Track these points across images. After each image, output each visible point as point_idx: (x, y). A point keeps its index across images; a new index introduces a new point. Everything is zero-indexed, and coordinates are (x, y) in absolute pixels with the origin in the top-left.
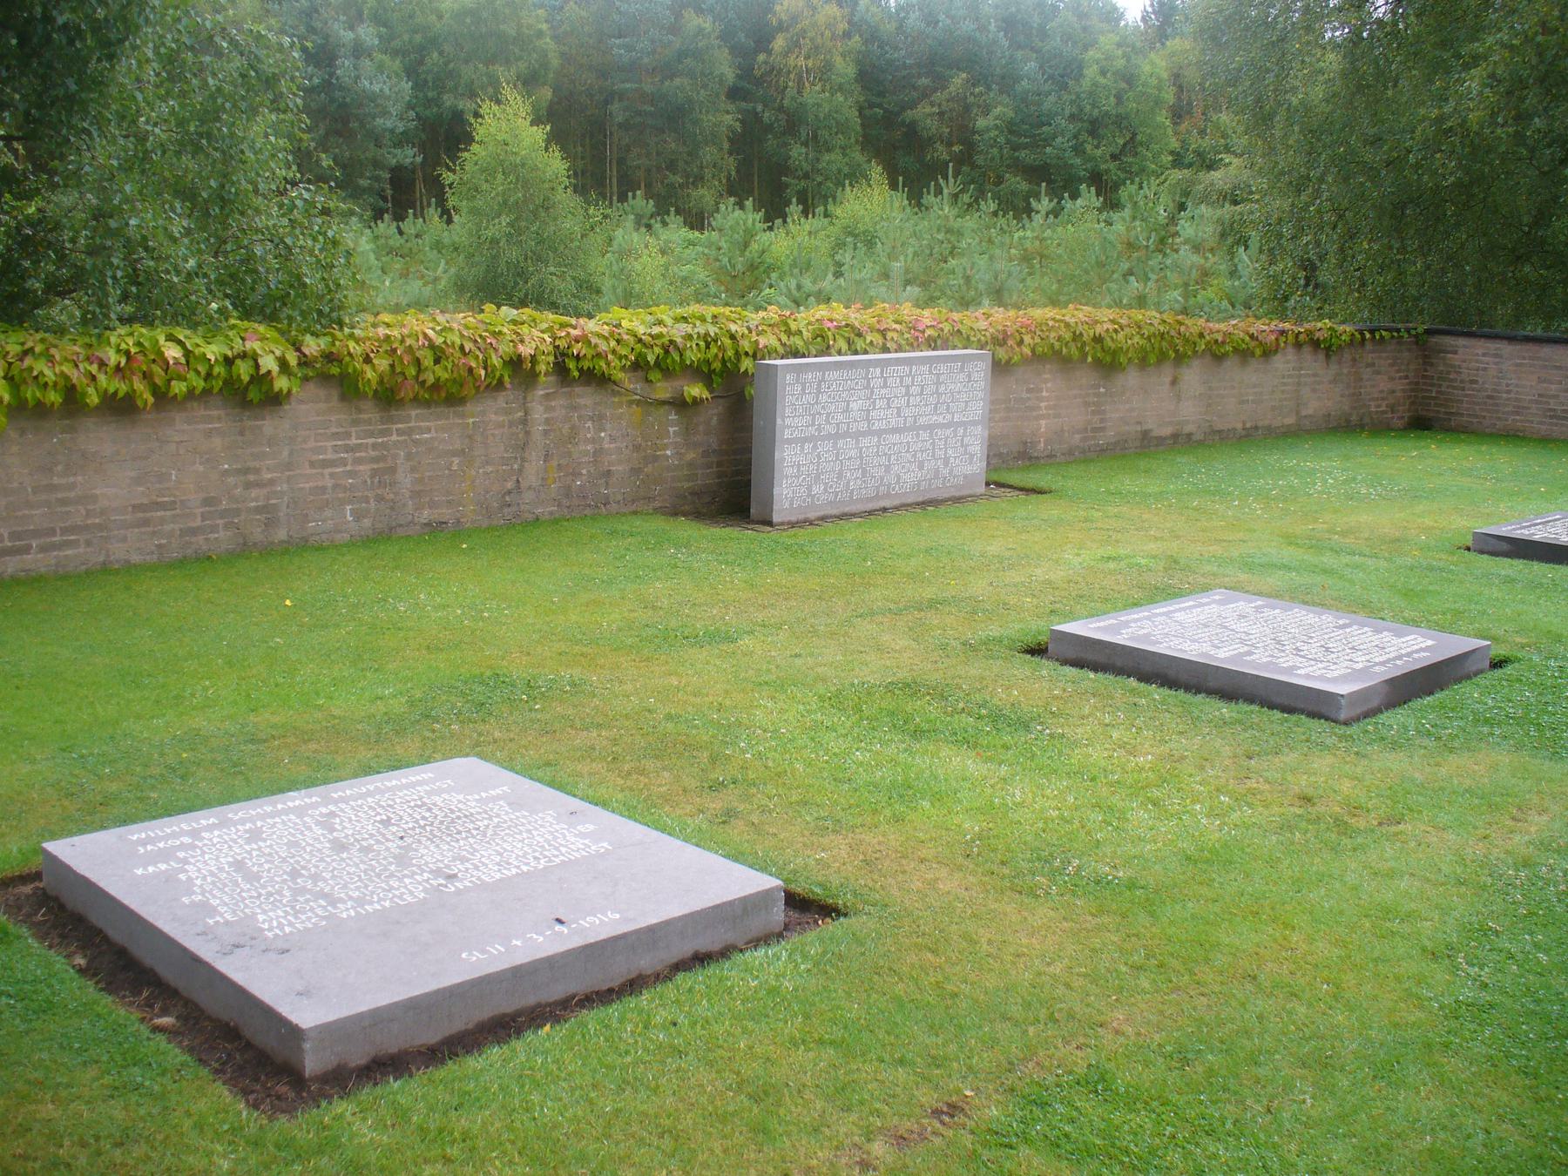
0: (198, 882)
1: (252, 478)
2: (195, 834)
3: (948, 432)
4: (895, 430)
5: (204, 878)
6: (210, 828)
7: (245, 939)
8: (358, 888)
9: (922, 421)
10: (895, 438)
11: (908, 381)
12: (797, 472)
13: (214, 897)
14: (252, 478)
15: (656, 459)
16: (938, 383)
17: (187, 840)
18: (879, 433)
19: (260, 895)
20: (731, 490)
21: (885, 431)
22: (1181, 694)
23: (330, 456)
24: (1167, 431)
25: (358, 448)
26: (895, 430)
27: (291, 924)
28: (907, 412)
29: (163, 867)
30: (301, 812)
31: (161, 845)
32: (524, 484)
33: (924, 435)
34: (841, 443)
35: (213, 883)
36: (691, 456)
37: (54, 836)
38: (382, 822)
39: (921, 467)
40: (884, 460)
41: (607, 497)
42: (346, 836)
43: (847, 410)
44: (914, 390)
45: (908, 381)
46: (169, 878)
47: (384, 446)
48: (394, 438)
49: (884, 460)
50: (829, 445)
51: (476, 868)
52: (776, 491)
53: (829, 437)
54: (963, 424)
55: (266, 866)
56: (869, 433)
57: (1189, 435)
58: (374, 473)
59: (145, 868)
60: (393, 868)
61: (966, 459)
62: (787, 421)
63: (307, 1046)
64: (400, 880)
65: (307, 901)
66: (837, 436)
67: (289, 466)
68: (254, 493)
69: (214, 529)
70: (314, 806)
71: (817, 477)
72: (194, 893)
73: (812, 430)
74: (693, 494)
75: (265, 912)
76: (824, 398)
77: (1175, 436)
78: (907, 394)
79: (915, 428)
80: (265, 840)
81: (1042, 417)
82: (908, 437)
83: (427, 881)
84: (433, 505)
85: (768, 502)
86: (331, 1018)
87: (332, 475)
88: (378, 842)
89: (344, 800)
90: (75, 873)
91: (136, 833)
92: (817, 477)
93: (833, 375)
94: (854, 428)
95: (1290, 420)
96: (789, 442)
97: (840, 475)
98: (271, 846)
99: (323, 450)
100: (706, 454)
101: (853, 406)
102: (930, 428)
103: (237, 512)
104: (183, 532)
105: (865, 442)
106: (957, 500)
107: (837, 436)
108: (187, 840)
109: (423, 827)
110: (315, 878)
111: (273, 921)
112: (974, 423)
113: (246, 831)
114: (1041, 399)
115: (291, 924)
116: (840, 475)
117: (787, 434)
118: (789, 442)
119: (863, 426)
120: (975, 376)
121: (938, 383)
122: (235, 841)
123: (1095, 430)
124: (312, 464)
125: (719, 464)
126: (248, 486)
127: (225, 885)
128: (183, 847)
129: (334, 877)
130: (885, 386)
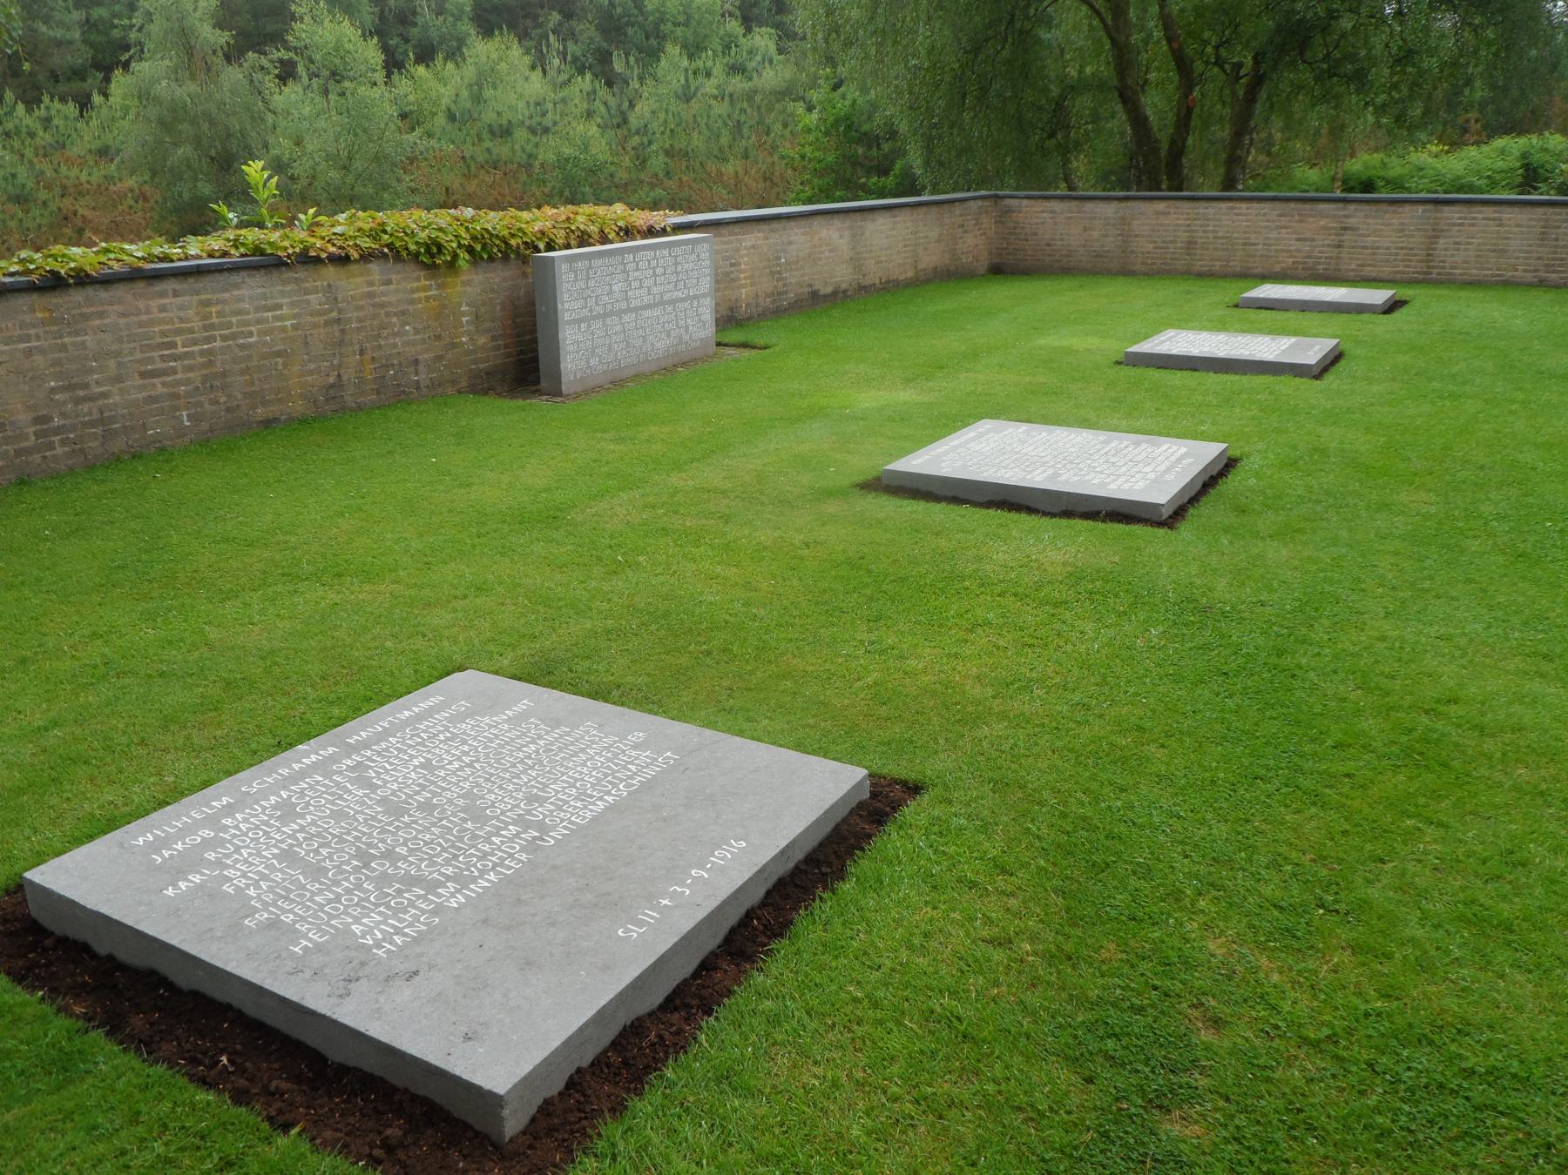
0: (252, 892)
1: (81, 393)
2: (212, 821)
3: (687, 304)
4: (649, 307)
5: (258, 887)
6: (230, 810)
7: (356, 966)
8: (447, 862)
9: (666, 297)
10: (647, 313)
11: (654, 263)
12: (579, 347)
13: (284, 911)
14: (81, 393)
15: (454, 346)
16: (676, 264)
17: (207, 833)
18: (637, 309)
19: (338, 896)
20: (522, 363)
21: (641, 308)
22: (943, 505)
23: (159, 365)
24: (829, 290)
25: (186, 355)
26: (649, 307)
27: (398, 931)
28: (655, 290)
29: (197, 879)
30: (322, 767)
31: (179, 846)
32: (345, 378)
33: (669, 309)
34: (608, 321)
35: (271, 890)
36: (482, 340)
37: (40, 858)
38: (422, 766)
39: (669, 336)
40: (641, 332)
41: (417, 382)
42: (394, 793)
43: (611, 292)
44: (659, 271)
45: (654, 263)
46: (209, 892)
47: (210, 352)
48: (218, 344)
49: (641, 332)
50: (599, 324)
51: (560, 809)
52: (562, 366)
53: (598, 316)
54: (696, 297)
55: (324, 851)
56: (629, 310)
57: (845, 292)
58: (205, 378)
59: (175, 886)
60: (469, 825)
61: (700, 324)
62: (566, 306)
63: (506, 1112)
64: (488, 840)
65: (399, 892)
66: (605, 315)
67: (118, 379)
68: (85, 407)
69: (51, 446)
70: (334, 759)
71: (593, 351)
72: (256, 910)
73: (586, 312)
74: (487, 374)
75: (357, 920)
76: (592, 283)
77: (835, 293)
78: (655, 275)
79: (662, 303)
80: (303, 816)
81: (744, 286)
82: (657, 312)
83: (517, 835)
84: (264, 403)
85: (556, 375)
86: (526, 1068)
87: (164, 384)
88: (435, 794)
89: (366, 745)
90: (84, 908)
91: (140, 835)
92: (593, 351)
93: (597, 263)
94: (617, 306)
95: (910, 274)
96: (569, 322)
97: (610, 349)
98: (313, 823)
99: (151, 360)
100: (494, 338)
101: (615, 288)
102: (672, 302)
103: (73, 428)
104: (18, 453)
105: (626, 318)
106: (695, 361)
107: (605, 315)
108: (207, 833)
109: (470, 765)
110: (389, 855)
111: (376, 930)
112: (704, 296)
113: (275, 807)
114: (740, 272)
115: (398, 931)
116: (610, 349)
117: (567, 317)
118: (569, 322)
119: (624, 305)
120: (703, 256)
121: (676, 264)
122: (266, 823)
123: (779, 294)
124: (143, 375)
125: (506, 346)
126: (78, 401)
127: (288, 891)
128: (207, 844)
129: (411, 850)
130: (637, 269)
